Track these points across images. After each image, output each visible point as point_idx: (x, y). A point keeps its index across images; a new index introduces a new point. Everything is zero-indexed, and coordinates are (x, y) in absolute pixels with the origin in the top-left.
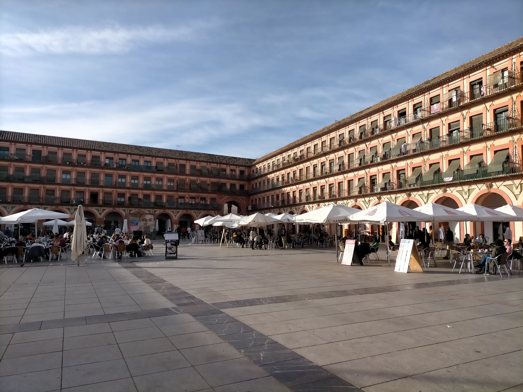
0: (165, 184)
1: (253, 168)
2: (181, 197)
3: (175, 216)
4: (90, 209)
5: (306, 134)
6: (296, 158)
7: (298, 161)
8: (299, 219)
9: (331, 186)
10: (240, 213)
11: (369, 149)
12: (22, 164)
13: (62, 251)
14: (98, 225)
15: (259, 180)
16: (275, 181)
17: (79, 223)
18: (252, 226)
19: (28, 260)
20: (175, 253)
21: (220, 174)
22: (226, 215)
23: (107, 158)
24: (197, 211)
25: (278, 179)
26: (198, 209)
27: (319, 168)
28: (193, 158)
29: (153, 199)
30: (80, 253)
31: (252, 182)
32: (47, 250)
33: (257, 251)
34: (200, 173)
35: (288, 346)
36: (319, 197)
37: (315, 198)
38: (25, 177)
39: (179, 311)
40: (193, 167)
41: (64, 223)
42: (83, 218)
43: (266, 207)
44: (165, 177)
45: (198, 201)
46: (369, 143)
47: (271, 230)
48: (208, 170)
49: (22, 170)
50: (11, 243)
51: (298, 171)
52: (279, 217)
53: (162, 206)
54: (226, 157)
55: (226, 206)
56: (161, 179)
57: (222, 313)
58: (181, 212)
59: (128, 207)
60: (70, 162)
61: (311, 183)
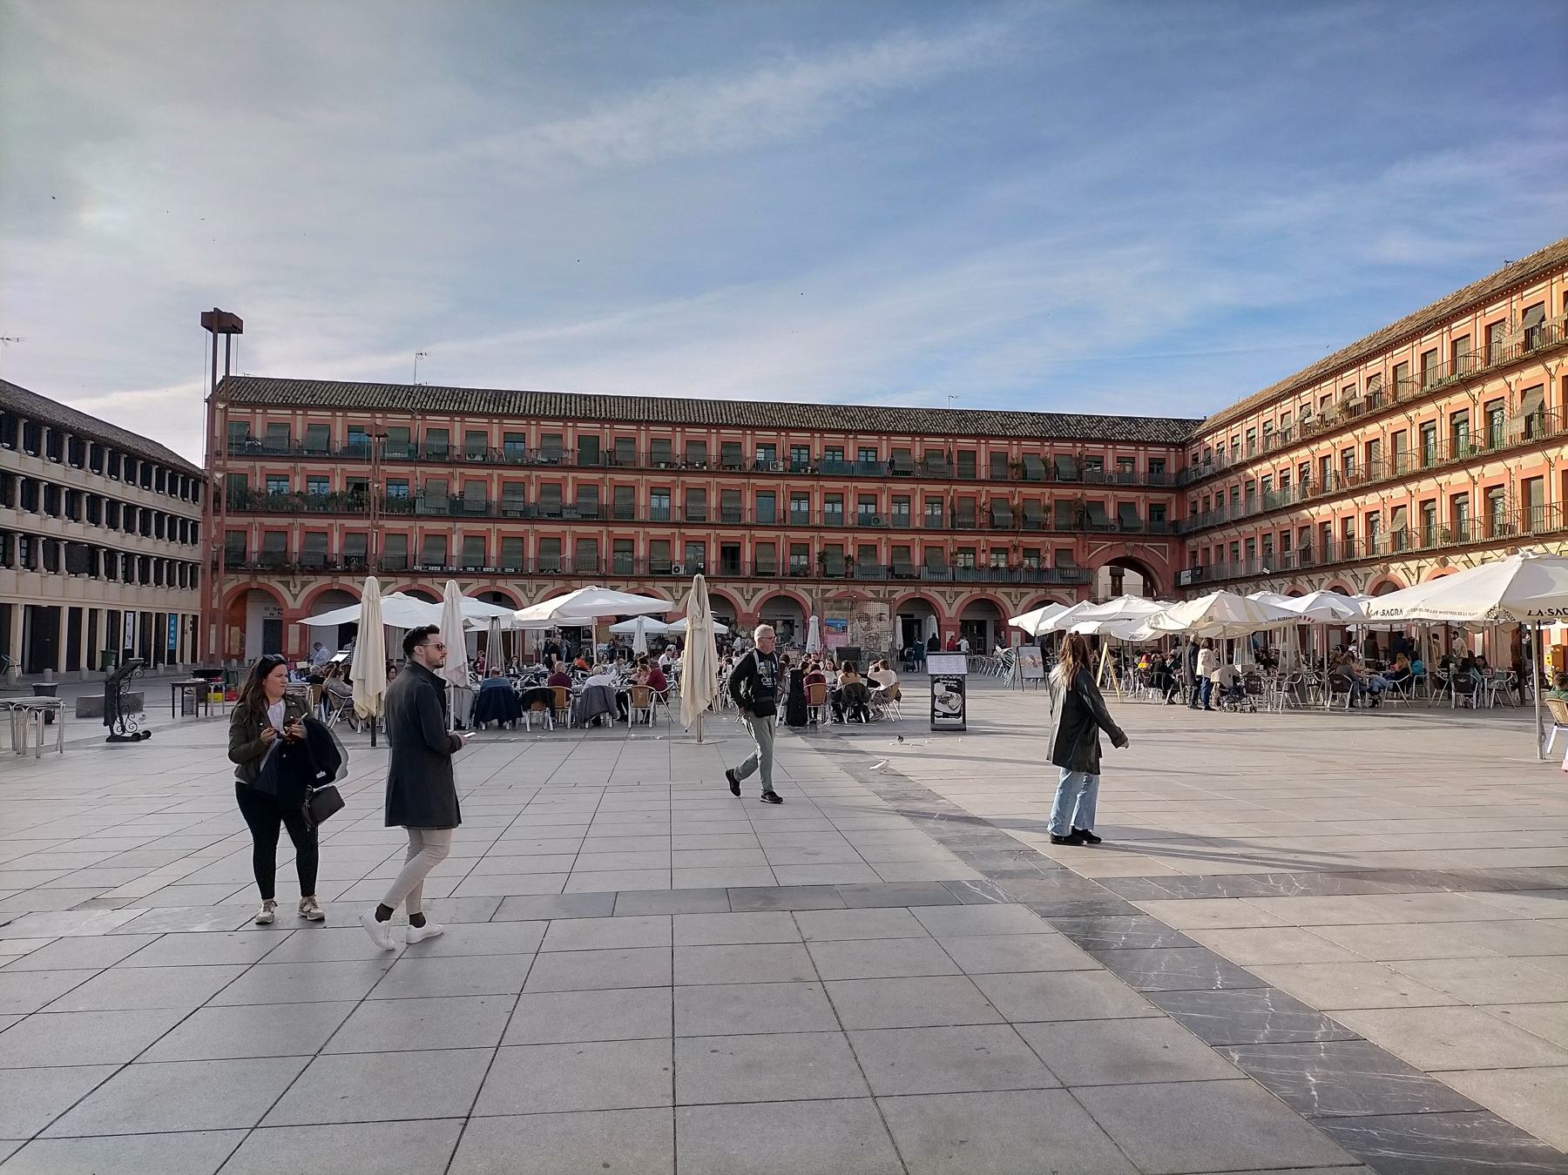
0: (918, 511)
1: (1195, 448)
2: (962, 550)
3: (950, 605)
4: (723, 588)
5: (1392, 318)
6: (1352, 404)
7: (1357, 415)
8: (1380, 609)
9: (1491, 496)
10: (1149, 592)
11: (1518, 395)
12: (558, 475)
13: (659, 699)
14: (744, 634)
15: (1218, 484)
16: (1275, 486)
17: (699, 627)
18: (1203, 634)
19: (578, 724)
20: (958, 715)
21: (1082, 473)
22: (1107, 600)
23: (759, 446)
24: (1012, 590)
25: (1284, 481)
26: (1017, 585)
27: (1443, 432)
28: (998, 430)
29: (884, 558)
30: (703, 706)
31: (1192, 494)
32: (622, 698)
33: (1221, 718)
34: (1020, 474)
35: (1409, 1055)
36: (1447, 536)
37: (1427, 539)
38: (563, 507)
39: (992, 892)
40: (997, 458)
41: (657, 626)
42: (708, 612)
43: (1243, 572)
44: (918, 490)
45: (1015, 560)
46: (1479, 389)
47: (1265, 651)
48: (1045, 462)
49: (556, 489)
50: (537, 677)
51: (1362, 448)
52: (1299, 605)
53: (911, 576)
54: (1101, 419)
55: (1104, 575)
56: (907, 499)
57: (1138, 913)
58: (966, 594)
59: (818, 582)
60: (667, 464)
61: (1412, 486)
